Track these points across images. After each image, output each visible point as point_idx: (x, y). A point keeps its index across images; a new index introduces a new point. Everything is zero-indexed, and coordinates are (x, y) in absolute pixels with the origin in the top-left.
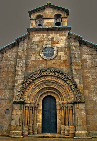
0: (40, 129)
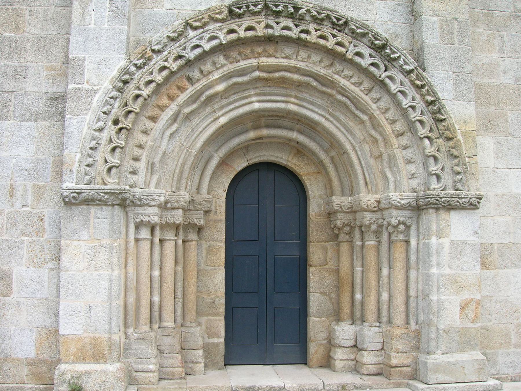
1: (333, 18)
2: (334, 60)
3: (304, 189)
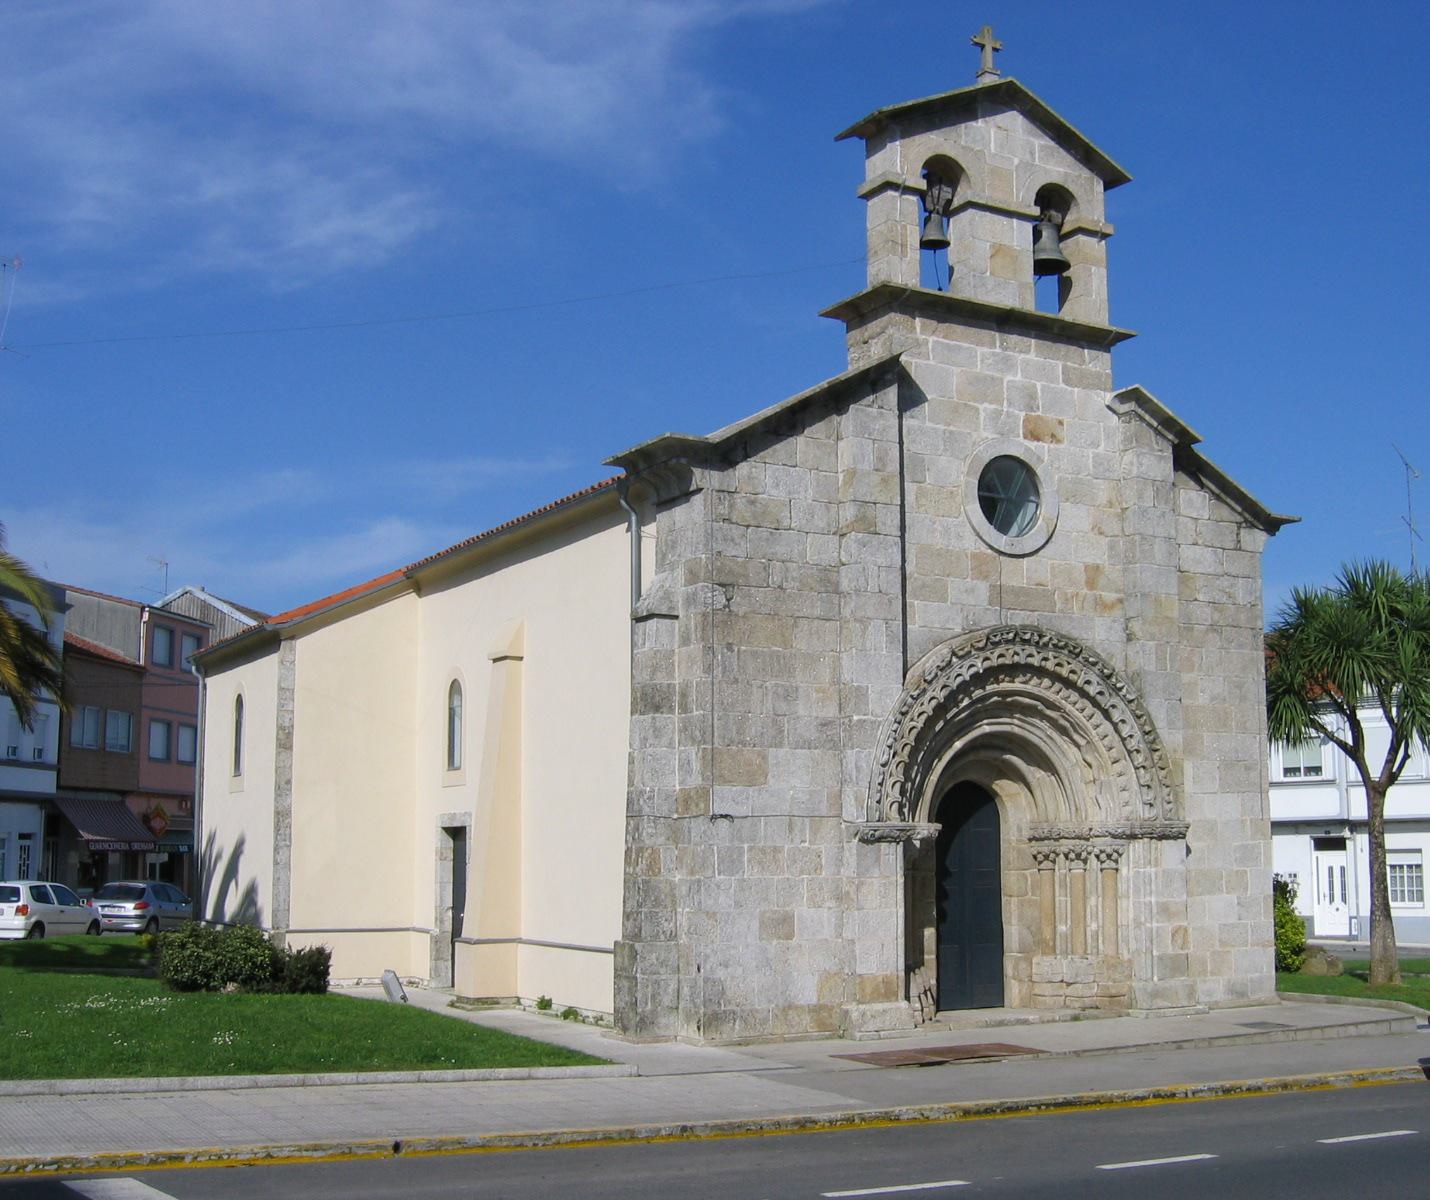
3: (107, 659)
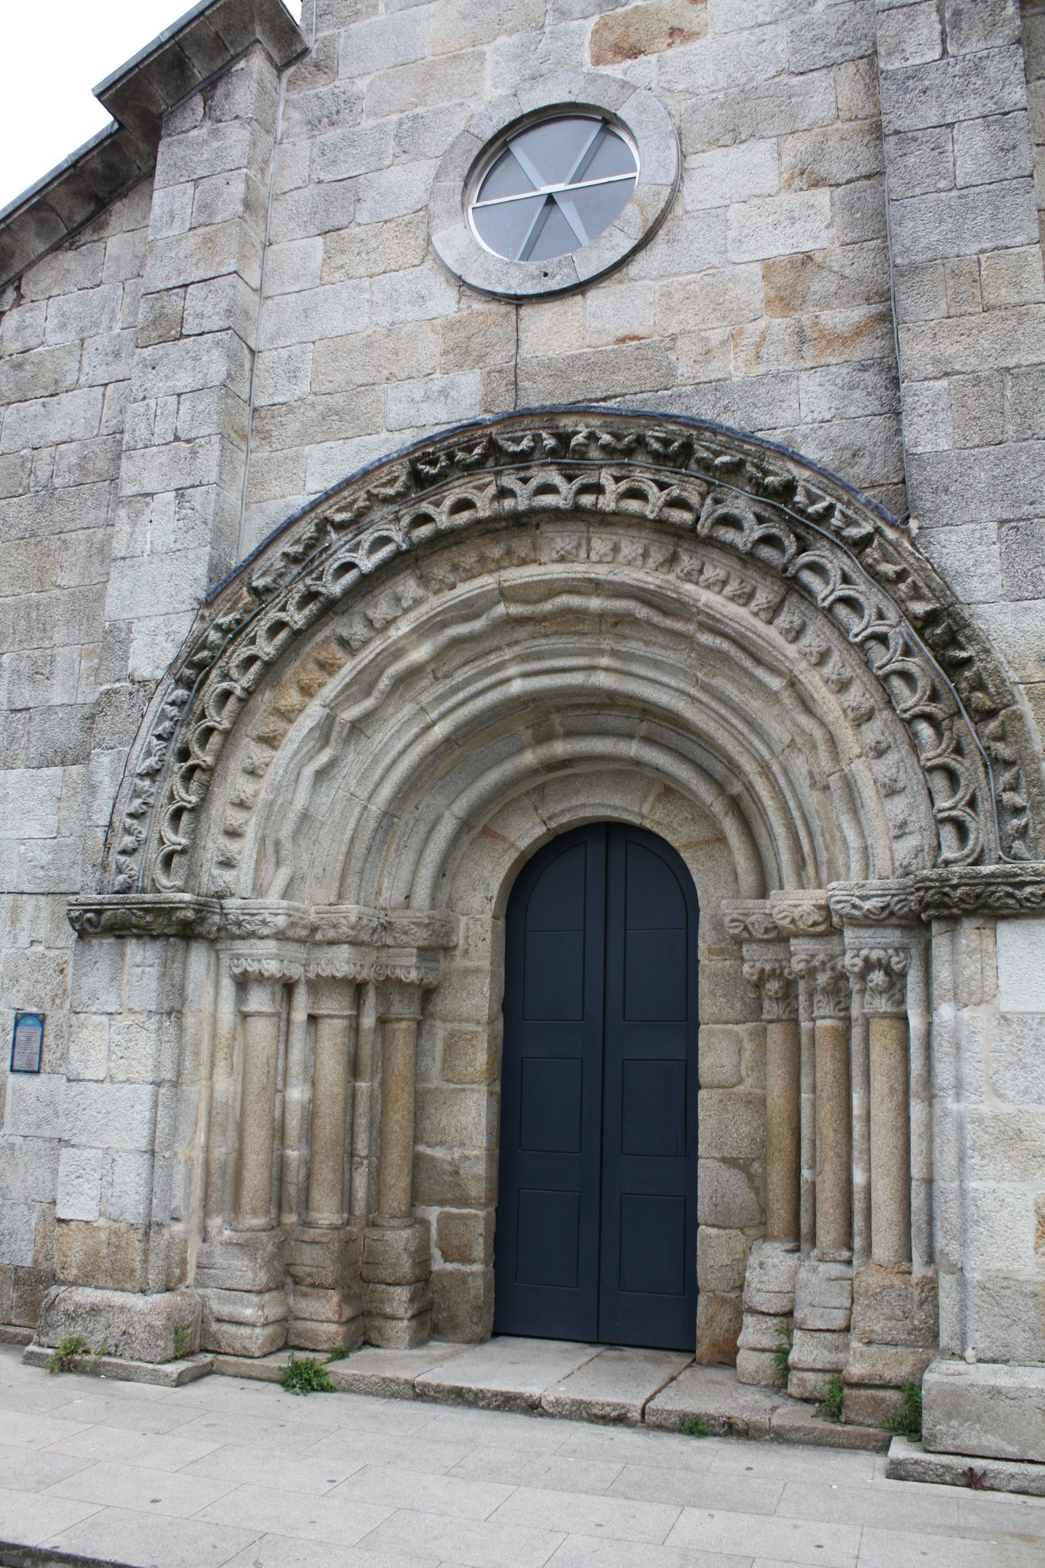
0: (464, 1278)
1: (652, 441)
2: (676, 545)
